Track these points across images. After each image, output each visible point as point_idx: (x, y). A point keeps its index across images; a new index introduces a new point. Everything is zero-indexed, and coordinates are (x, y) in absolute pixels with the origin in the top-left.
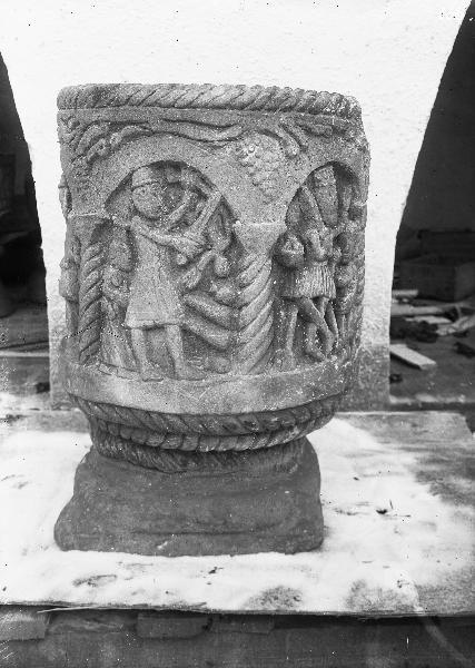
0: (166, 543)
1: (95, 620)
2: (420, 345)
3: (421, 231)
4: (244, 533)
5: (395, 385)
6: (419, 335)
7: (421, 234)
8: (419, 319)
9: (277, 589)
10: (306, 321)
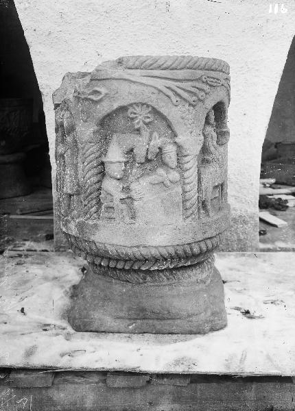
0: (134, 325)
1: (82, 376)
2: (277, 212)
3: (277, 143)
4: (180, 318)
5: (262, 236)
6: (276, 206)
7: (277, 145)
8: (277, 197)
9: (183, 358)
10: (212, 200)
